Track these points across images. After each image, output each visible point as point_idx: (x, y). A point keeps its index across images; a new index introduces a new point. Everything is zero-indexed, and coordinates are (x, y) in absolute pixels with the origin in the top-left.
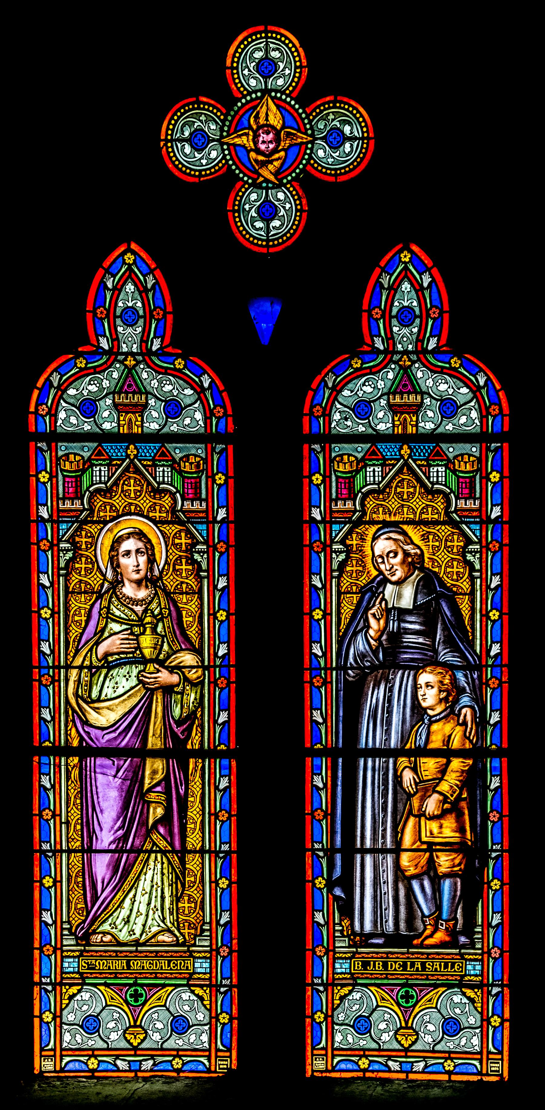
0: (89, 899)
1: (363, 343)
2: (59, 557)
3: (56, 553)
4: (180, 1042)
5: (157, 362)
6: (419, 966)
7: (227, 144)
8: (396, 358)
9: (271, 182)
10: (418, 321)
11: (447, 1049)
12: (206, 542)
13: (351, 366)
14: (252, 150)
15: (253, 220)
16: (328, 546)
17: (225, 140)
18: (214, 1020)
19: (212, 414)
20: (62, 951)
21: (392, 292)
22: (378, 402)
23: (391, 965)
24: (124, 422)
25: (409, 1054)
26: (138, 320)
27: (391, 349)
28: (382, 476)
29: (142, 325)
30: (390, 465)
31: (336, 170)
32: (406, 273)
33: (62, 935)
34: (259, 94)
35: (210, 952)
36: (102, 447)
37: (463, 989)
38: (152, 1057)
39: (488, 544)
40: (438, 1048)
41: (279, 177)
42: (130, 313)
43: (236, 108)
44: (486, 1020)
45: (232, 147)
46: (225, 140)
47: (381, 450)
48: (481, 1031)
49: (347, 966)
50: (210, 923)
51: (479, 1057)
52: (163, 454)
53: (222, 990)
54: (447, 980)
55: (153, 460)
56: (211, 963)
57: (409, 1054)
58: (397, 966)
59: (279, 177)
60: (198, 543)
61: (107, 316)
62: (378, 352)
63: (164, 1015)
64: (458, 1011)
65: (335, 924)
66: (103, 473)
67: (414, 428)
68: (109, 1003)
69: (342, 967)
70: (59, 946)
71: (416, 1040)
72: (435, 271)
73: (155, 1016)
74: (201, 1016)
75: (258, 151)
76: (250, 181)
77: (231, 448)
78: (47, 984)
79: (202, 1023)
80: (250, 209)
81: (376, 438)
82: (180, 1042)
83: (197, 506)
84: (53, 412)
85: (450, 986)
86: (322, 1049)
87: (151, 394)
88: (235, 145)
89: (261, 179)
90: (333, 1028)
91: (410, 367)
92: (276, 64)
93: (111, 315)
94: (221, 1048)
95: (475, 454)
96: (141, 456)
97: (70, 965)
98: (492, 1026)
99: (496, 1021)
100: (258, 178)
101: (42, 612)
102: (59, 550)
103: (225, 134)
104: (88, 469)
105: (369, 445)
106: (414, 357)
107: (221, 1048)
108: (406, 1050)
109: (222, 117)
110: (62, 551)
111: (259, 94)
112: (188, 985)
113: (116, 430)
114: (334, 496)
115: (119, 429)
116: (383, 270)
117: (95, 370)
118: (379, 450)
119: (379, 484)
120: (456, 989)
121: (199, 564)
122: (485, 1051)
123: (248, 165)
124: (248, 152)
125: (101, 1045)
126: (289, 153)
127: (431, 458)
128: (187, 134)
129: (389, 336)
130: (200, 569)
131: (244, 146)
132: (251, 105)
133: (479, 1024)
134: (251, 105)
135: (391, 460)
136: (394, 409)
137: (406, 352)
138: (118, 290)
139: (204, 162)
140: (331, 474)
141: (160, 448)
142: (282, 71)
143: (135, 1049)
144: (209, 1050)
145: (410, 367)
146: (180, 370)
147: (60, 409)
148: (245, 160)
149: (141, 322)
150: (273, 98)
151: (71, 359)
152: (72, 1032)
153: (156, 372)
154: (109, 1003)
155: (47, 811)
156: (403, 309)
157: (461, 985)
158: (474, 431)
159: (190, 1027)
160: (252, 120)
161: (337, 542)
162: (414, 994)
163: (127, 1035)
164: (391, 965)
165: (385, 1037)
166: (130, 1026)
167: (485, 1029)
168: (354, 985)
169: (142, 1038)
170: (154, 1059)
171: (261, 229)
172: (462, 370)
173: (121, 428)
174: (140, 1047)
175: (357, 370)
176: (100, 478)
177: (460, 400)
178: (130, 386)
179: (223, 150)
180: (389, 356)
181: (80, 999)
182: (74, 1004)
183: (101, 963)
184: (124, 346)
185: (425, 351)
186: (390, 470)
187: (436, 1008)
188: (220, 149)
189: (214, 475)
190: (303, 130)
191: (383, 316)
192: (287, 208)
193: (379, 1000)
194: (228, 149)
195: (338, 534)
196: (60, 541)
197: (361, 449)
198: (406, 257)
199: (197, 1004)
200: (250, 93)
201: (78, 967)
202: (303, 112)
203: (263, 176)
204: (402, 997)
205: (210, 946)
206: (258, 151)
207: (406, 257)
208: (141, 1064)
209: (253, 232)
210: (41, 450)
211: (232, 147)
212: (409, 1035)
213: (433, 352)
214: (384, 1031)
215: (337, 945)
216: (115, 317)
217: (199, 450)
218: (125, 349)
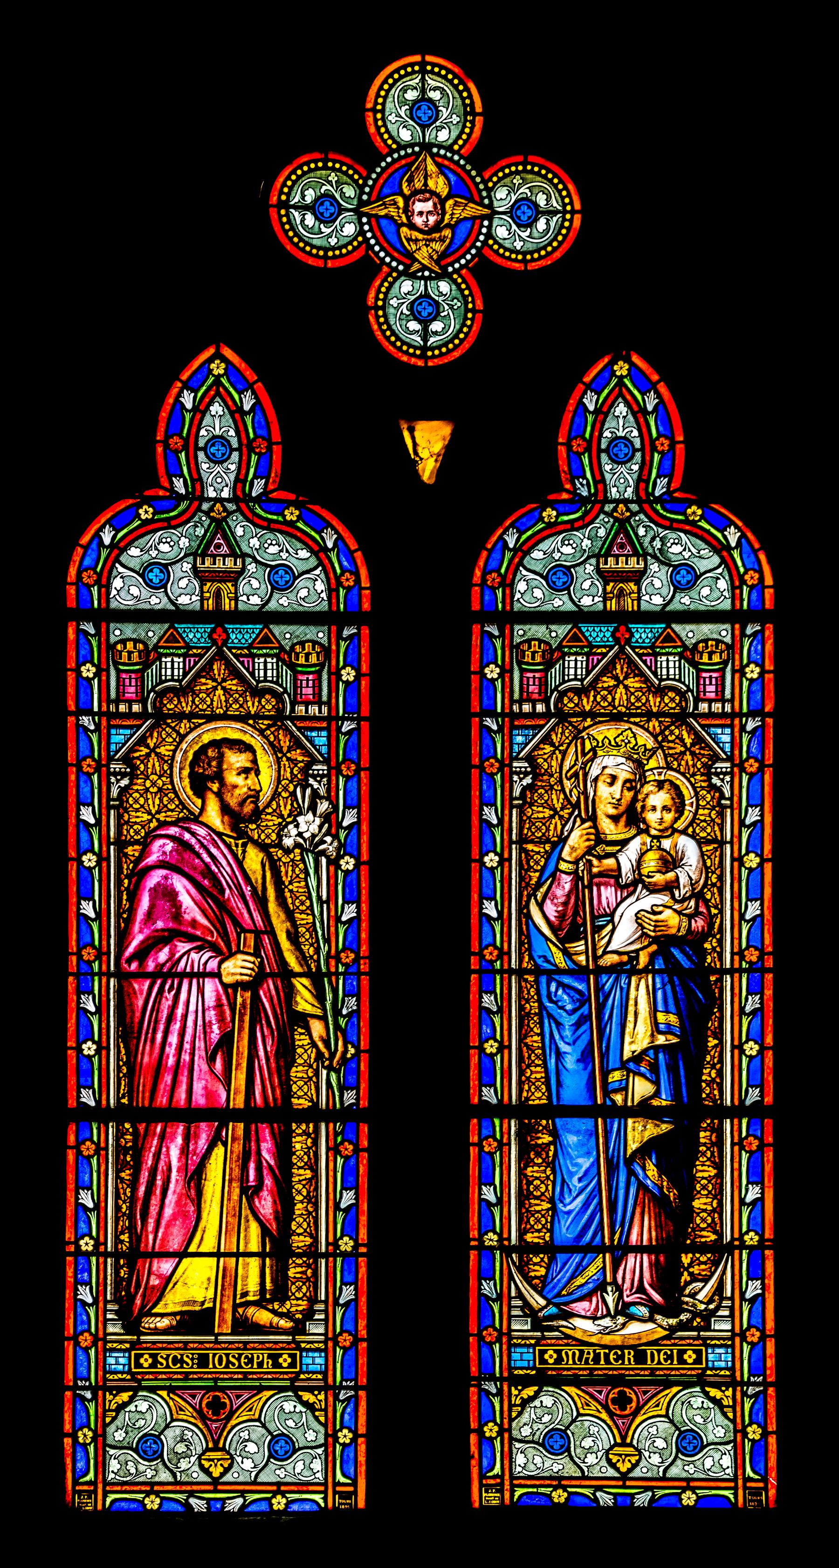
1: (158, 485)
2: (511, 782)
3: (507, 778)
4: (281, 1473)
5: (259, 511)
7: (367, 215)
8: (608, 508)
9: (431, 271)
10: (638, 455)
11: (684, 1475)
12: (326, 761)
13: (138, 516)
14: (403, 224)
16: (507, 765)
17: (486, 211)
18: (330, 1440)
19: (339, 584)
20: (105, 1342)
21: (601, 417)
22: (179, 565)
23: (652, 1354)
24: (208, 595)
25: (628, 1483)
26: (230, 454)
27: (198, 493)
28: (184, 668)
29: (237, 460)
30: (194, 655)
32: (620, 390)
33: (510, 1317)
34: (417, 149)
35: (732, 1338)
36: (176, 629)
37: (707, 1389)
38: (242, 1493)
39: (742, 762)
40: (262, 1478)
41: (443, 263)
43: (378, 170)
44: (332, 1437)
46: (486, 211)
47: (587, 634)
48: (326, 1451)
49: (530, 1357)
50: (732, 1298)
51: (322, 1488)
52: (668, 639)
53: (751, 1391)
54: (717, 1375)
55: (653, 647)
56: (733, 1354)
57: (628, 1483)
58: (662, 1357)
59: (443, 263)
60: (315, 761)
61: (185, 447)
62: (180, 498)
63: (664, 1426)
64: (290, 1423)
65: (510, 1298)
66: (579, 664)
67: (233, 602)
68: (663, 1412)
69: (117, 1361)
70: (505, 1330)
71: (231, 1466)
72: (662, 388)
73: (653, 1430)
74: (314, 1435)
75: (412, 226)
76: (401, 268)
77: (365, 631)
78: (84, 1388)
79: (314, 1444)
81: (578, 617)
82: (281, 1473)
83: (314, 710)
84: (104, 581)
85: (686, 1385)
86: (495, 1477)
87: (249, 556)
88: (376, 216)
89: (416, 266)
90: (105, 1452)
91: (224, 519)
93: (592, 447)
94: (752, 1475)
95: (725, 640)
96: (637, 642)
97: (117, 1361)
98: (749, 1440)
99: (345, 1436)
100: (411, 265)
101: (84, 858)
102: (109, 774)
104: (557, 661)
105: (569, 627)
106: (231, 507)
107: (752, 1475)
108: (624, 1477)
109: (361, 182)
110: (518, 774)
111: (435, 150)
112: (295, 1390)
113: (600, 607)
114: (113, 695)
115: (605, 606)
116: (588, 387)
117: (572, 525)
118: (583, 633)
119: (582, 680)
120: (290, 1393)
121: (719, 790)
122: (330, 1480)
123: (398, 246)
124: (399, 226)
125: (574, 1472)
126: (458, 231)
127: (657, 644)
129: (598, 478)
130: (722, 796)
133: (321, 1441)
135: (197, 648)
136: (605, 576)
137: (219, 500)
138: (603, 413)
140: (108, 666)
141: (665, 629)
143: (216, 1482)
144: (325, 1484)
145: (224, 519)
146: (292, 524)
147: (518, 578)
148: (393, 238)
149: (235, 456)
150: (433, 156)
151: (534, 509)
152: (122, 1458)
153: (255, 525)
154: (663, 1412)
155: (88, 1143)
156: (214, 439)
157: (702, 1381)
158: (318, 609)
159: (295, 1451)
160: (405, 185)
161: (118, 760)
162: (227, 1401)
163: (203, 1462)
164: (652, 1354)
165: (591, 1459)
166: (616, 1444)
167: (330, 1450)
168: (136, 1390)
169: (226, 1465)
170: (244, 1497)
172: (300, 525)
173: (608, 603)
174: (631, 1475)
175: (146, 522)
176: (265, 673)
177: (702, 566)
178: (218, 546)
179: (362, 225)
180: (196, 503)
181: (133, 1409)
182: (123, 1418)
183: (570, 1353)
184: (614, 490)
185: (248, 498)
186: (599, 661)
187: (667, 1416)
189: (742, 668)
190: (477, 198)
191: (588, 449)
193: (579, 1405)
195: (121, 748)
196: (110, 759)
197: (153, 633)
198: (621, 369)
199: (307, 1417)
200: (405, 147)
203: (420, 262)
204: (614, 1401)
205: (325, 1334)
206: (412, 226)
207: (218, 368)
208: (224, 1503)
209: (404, 336)
210: (491, 635)
212: (219, 1460)
213: (258, 499)
214: (589, 1450)
215: (514, 1327)
216: (197, 448)
217: (723, 631)
218: (614, 493)
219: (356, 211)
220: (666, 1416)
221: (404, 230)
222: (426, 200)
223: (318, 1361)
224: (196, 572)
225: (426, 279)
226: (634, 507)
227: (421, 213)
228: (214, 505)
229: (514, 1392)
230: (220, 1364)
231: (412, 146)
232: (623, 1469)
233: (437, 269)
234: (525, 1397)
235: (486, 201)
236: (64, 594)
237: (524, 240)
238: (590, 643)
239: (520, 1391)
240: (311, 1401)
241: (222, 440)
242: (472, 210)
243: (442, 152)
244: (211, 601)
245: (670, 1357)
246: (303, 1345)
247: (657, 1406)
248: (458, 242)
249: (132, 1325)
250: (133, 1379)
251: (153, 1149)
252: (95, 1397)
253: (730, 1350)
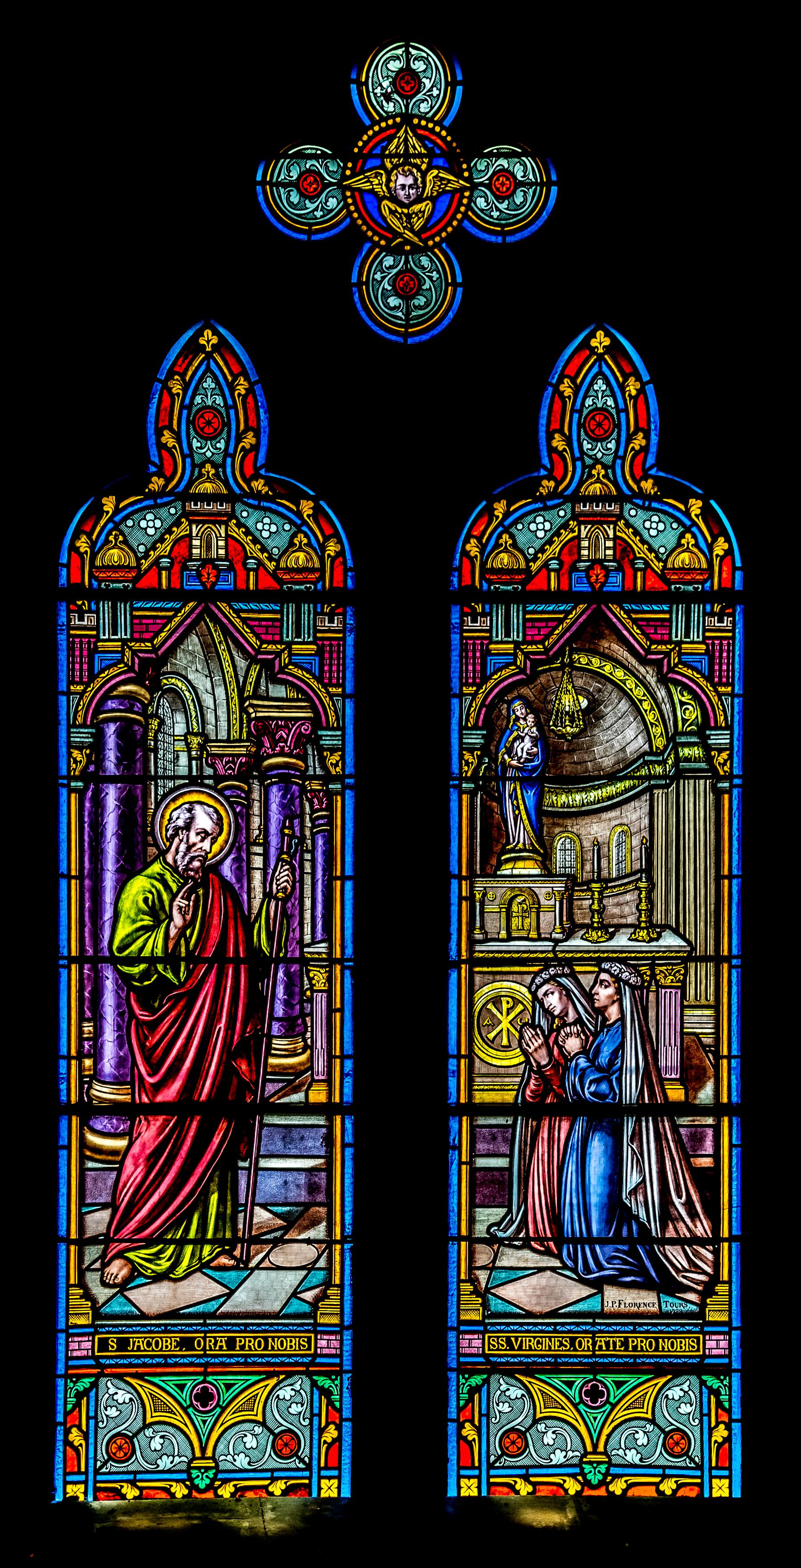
0: (113, 1227)
6: (224, 1344)
14: (384, 198)
15: (385, 297)
31: (503, 226)
34: (398, 120)
41: (424, 236)
42: (208, 416)
45: (357, 194)
49: (88, 1345)
75: (394, 199)
76: (383, 243)
80: (383, 278)
92: (394, 286)
103: (348, 172)
124: (380, 199)
128: (295, 174)
131: (372, 192)
132: (383, 135)
134: (383, 135)
139: (319, 214)
142: (429, 91)
150: (414, 128)
171: (395, 308)
179: (345, 198)
188: (340, 197)
192: (434, 279)
194: (352, 197)
201: (483, 1347)
202: (442, 239)
206: (394, 199)
211: (357, 194)
219: (339, 184)
223: (323, 1343)
225: (406, 254)
227: (403, 187)
229: (462, 1381)
230: (651, 1348)
231: (394, 117)
233: (416, 239)
234: (474, 1384)
235: (466, 174)
236: (58, 576)
237: (501, 211)
239: (466, 1380)
242: (455, 183)
243: (423, 123)
248: (438, 215)
250: (98, 1365)
251: (86, 814)
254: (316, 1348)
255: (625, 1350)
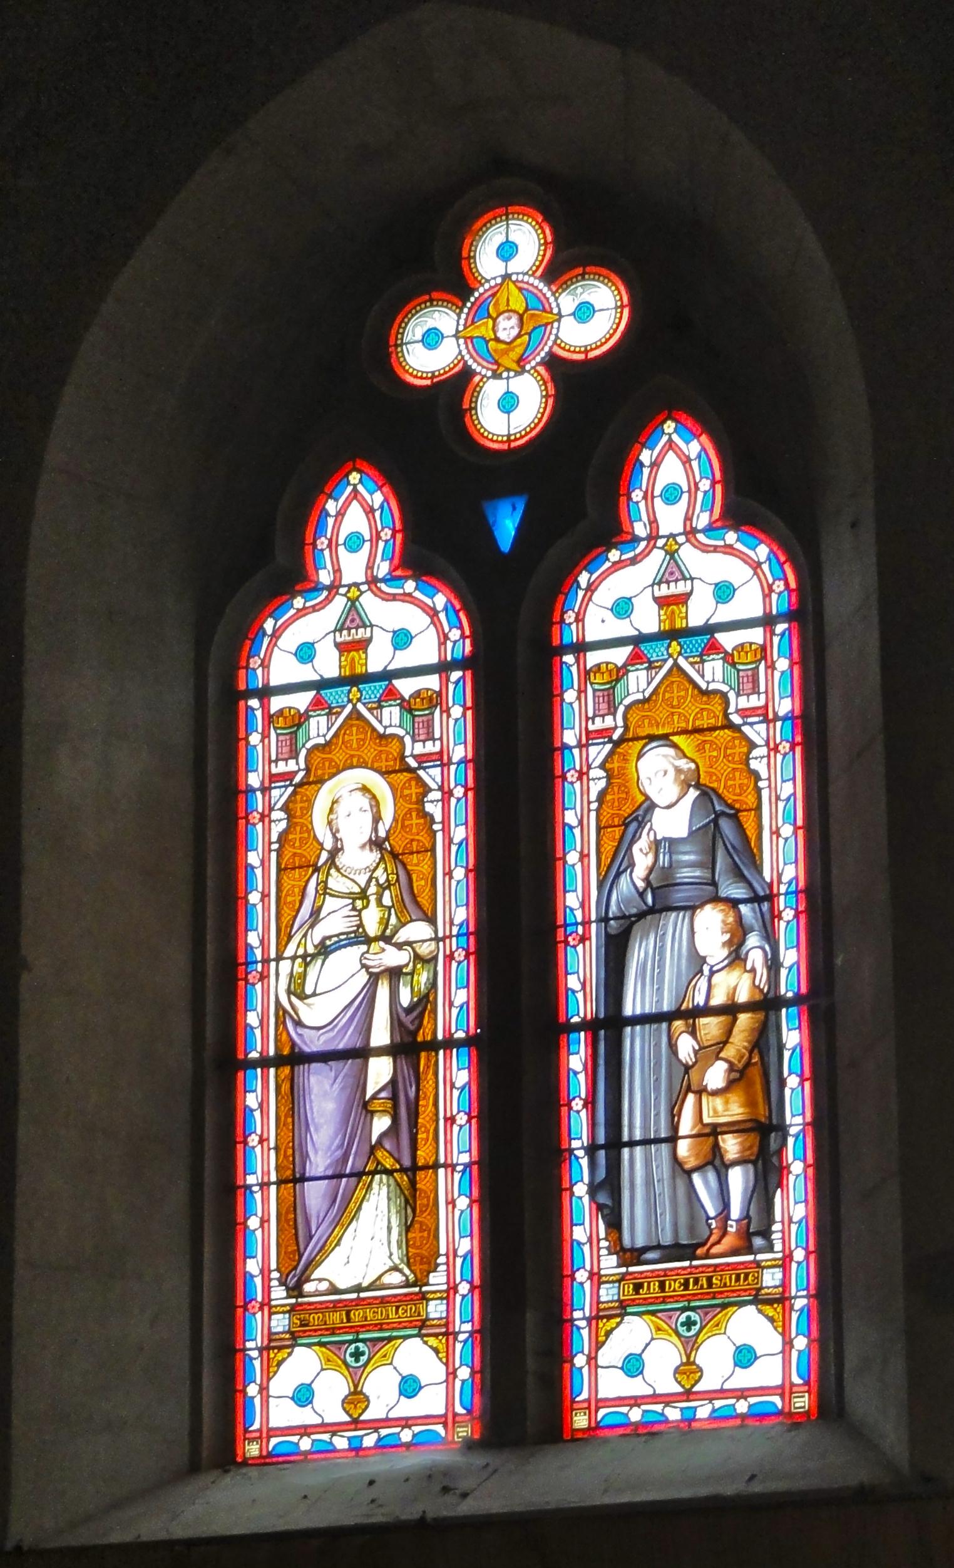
77: (469, 674)
118: (643, 652)
119: (324, 736)
196: (271, 809)
197: (619, 656)
220: (653, 1339)
221: (492, 344)
222: (509, 318)
224: (338, 645)
226: (364, 588)
228: (668, 541)
232: (688, 1387)
238: (649, 659)
240: (770, 1315)
241: (358, 535)
244: (667, 622)
245: (738, 1279)
246: (763, 1264)
247: (385, 1356)
249: (296, 1290)
252: (261, 1355)
253: (445, 1302)
254: (619, 1287)
255: (683, 1290)
